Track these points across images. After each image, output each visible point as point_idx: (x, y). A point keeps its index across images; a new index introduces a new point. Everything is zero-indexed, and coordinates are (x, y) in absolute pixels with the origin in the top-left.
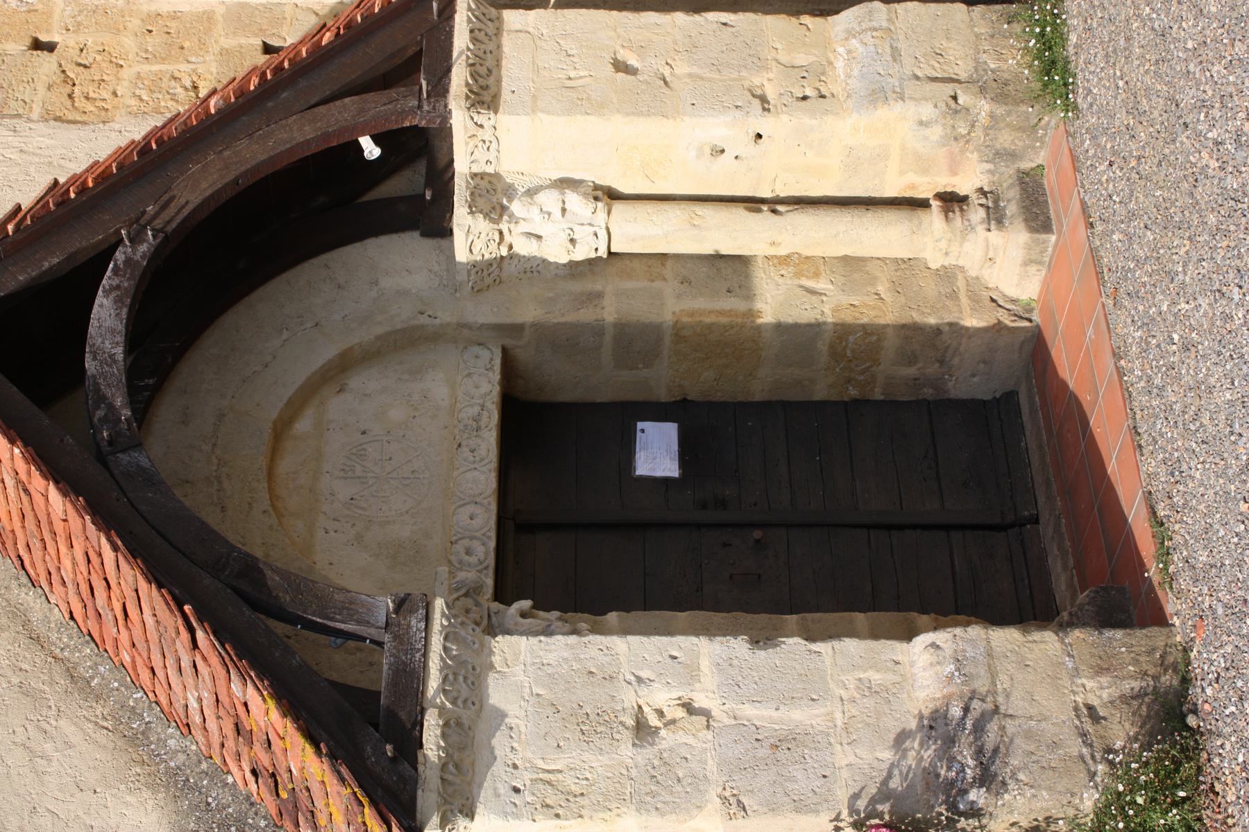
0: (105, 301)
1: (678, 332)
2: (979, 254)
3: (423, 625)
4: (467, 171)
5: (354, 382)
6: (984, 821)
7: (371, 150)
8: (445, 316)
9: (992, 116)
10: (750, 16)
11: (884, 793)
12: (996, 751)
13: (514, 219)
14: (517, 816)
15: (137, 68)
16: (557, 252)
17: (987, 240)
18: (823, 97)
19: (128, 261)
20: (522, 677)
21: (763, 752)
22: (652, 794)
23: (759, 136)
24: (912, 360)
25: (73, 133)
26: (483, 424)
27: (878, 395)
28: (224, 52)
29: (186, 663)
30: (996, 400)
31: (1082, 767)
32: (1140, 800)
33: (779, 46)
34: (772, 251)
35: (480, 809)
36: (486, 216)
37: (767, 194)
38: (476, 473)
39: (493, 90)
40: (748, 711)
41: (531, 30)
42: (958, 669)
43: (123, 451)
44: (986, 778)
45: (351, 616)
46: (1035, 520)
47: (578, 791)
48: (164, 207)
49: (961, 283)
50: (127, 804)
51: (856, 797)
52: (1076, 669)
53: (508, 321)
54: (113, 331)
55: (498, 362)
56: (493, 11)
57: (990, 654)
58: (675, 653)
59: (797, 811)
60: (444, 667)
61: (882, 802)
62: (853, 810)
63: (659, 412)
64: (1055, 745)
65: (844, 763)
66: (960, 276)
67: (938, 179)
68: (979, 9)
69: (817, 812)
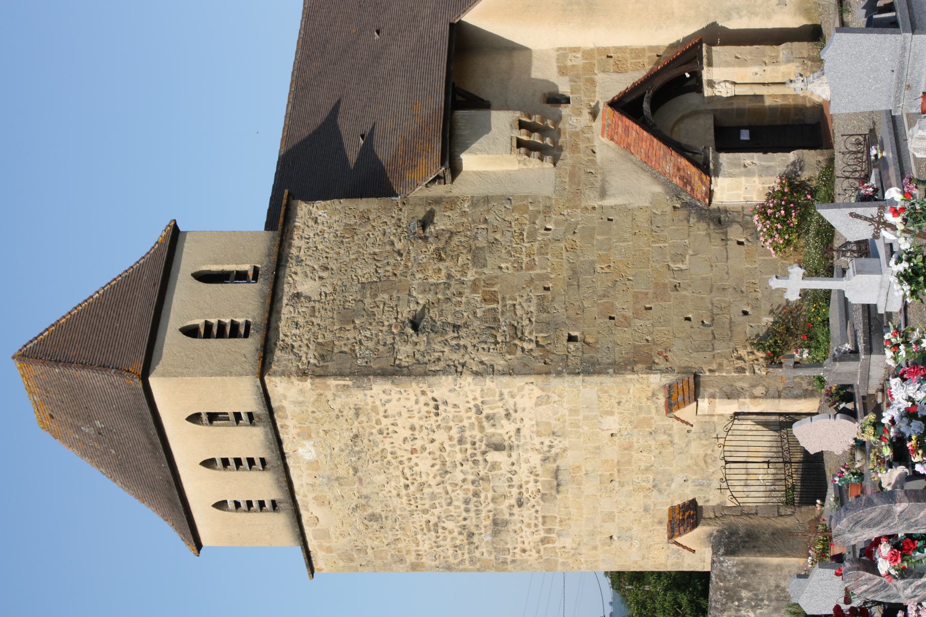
7: (688, 75)
11: (784, 173)
16: (724, 95)
25: (621, 75)
63: (745, 128)
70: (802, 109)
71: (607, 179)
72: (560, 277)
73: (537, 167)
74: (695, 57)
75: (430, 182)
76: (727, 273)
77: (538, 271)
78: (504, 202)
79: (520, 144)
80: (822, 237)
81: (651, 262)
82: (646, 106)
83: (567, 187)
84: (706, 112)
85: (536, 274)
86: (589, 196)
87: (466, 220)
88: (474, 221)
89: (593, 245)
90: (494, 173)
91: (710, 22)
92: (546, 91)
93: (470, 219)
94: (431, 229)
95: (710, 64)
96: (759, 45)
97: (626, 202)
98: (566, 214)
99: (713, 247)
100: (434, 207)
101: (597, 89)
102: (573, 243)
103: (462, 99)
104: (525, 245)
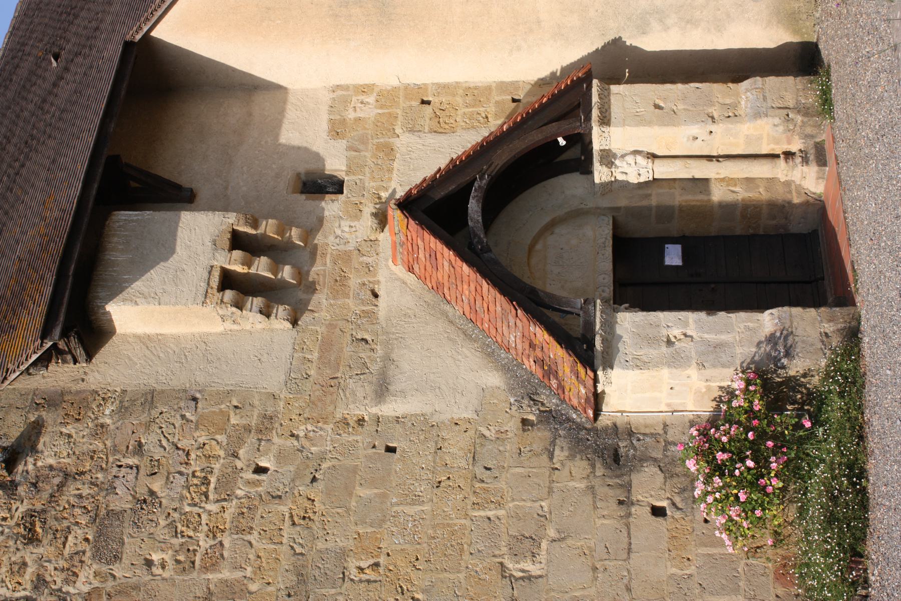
0: (473, 201)
1: (681, 209)
2: (799, 176)
3: (593, 308)
4: (598, 149)
5: (557, 230)
6: (787, 370)
7: (562, 142)
8: (591, 205)
9: (802, 121)
10: (708, 84)
11: (753, 361)
12: (791, 346)
13: (617, 167)
14: (628, 369)
15: (463, 110)
16: (633, 179)
17: (802, 170)
18: (736, 116)
19: (479, 186)
20: (627, 326)
21: (711, 349)
22: (673, 362)
23: (711, 132)
24: (774, 218)
25: (442, 138)
26: (607, 244)
27: (761, 232)
28: (497, 102)
29: (512, 323)
30: (809, 233)
31: (821, 351)
32: (838, 360)
33: (719, 96)
34: (717, 176)
35: (615, 367)
36: (606, 166)
37: (715, 154)
38: (604, 263)
39: (608, 118)
40: (706, 336)
41: (621, 93)
42: (779, 321)
43: (485, 253)
44: (787, 354)
45: (569, 305)
46: (823, 279)
47: (648, 361)
48: (490, 167)
49: (793, 187)
50: (488, 376)
51: (743, 363)
52: (822, 321)
53: (615, 206)
54: (477, 212)
55: (611, 222)
56: (607, 86)
57: (791, 316)
58: (680, 318)
59: (723, 367)
60: (601, 322)
61: (752, 364)
62: (741, 367)
63: (674, 241)
64: (812, 345)
65: (739, 352)
66: (793, 184)
67: (783, 146)
68: (799, 79)
69: (729, 367)
70: (784, 206)
71: (394, 356)
72: (270, 589)
73: (259, 326)
74: (579, 105)
75: (34, 364)
76: (629, 589)
77: (226, 574)
78: (182, 404)
79: (228, 280)
80: (840, 529)
81: (466, 556)
82: (474, 206)
83: (312, 372)
84: (598, 212)
85: (222, 581)
86: (354, 393)
87: (101, 446)
88: (115, 448)
89: (348, 510)
90: (177, 338)
91: (610, 37)
92: (302, 169)
93: (109, 443)
94: (28, 466)
95: (605, 121)
96: (701, 82)
97: (428, 410)
98: (302, 434)
99: (599, 522)
100: (44, 414)
101: (396, 165)
102: (308, 504)
103: (137, 185)
104: (209, 507)
